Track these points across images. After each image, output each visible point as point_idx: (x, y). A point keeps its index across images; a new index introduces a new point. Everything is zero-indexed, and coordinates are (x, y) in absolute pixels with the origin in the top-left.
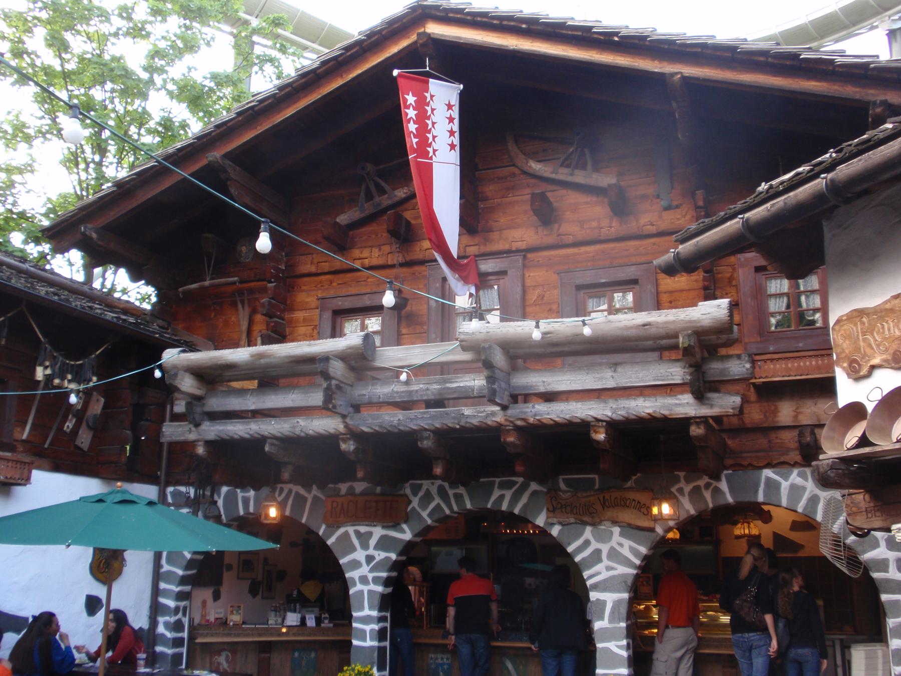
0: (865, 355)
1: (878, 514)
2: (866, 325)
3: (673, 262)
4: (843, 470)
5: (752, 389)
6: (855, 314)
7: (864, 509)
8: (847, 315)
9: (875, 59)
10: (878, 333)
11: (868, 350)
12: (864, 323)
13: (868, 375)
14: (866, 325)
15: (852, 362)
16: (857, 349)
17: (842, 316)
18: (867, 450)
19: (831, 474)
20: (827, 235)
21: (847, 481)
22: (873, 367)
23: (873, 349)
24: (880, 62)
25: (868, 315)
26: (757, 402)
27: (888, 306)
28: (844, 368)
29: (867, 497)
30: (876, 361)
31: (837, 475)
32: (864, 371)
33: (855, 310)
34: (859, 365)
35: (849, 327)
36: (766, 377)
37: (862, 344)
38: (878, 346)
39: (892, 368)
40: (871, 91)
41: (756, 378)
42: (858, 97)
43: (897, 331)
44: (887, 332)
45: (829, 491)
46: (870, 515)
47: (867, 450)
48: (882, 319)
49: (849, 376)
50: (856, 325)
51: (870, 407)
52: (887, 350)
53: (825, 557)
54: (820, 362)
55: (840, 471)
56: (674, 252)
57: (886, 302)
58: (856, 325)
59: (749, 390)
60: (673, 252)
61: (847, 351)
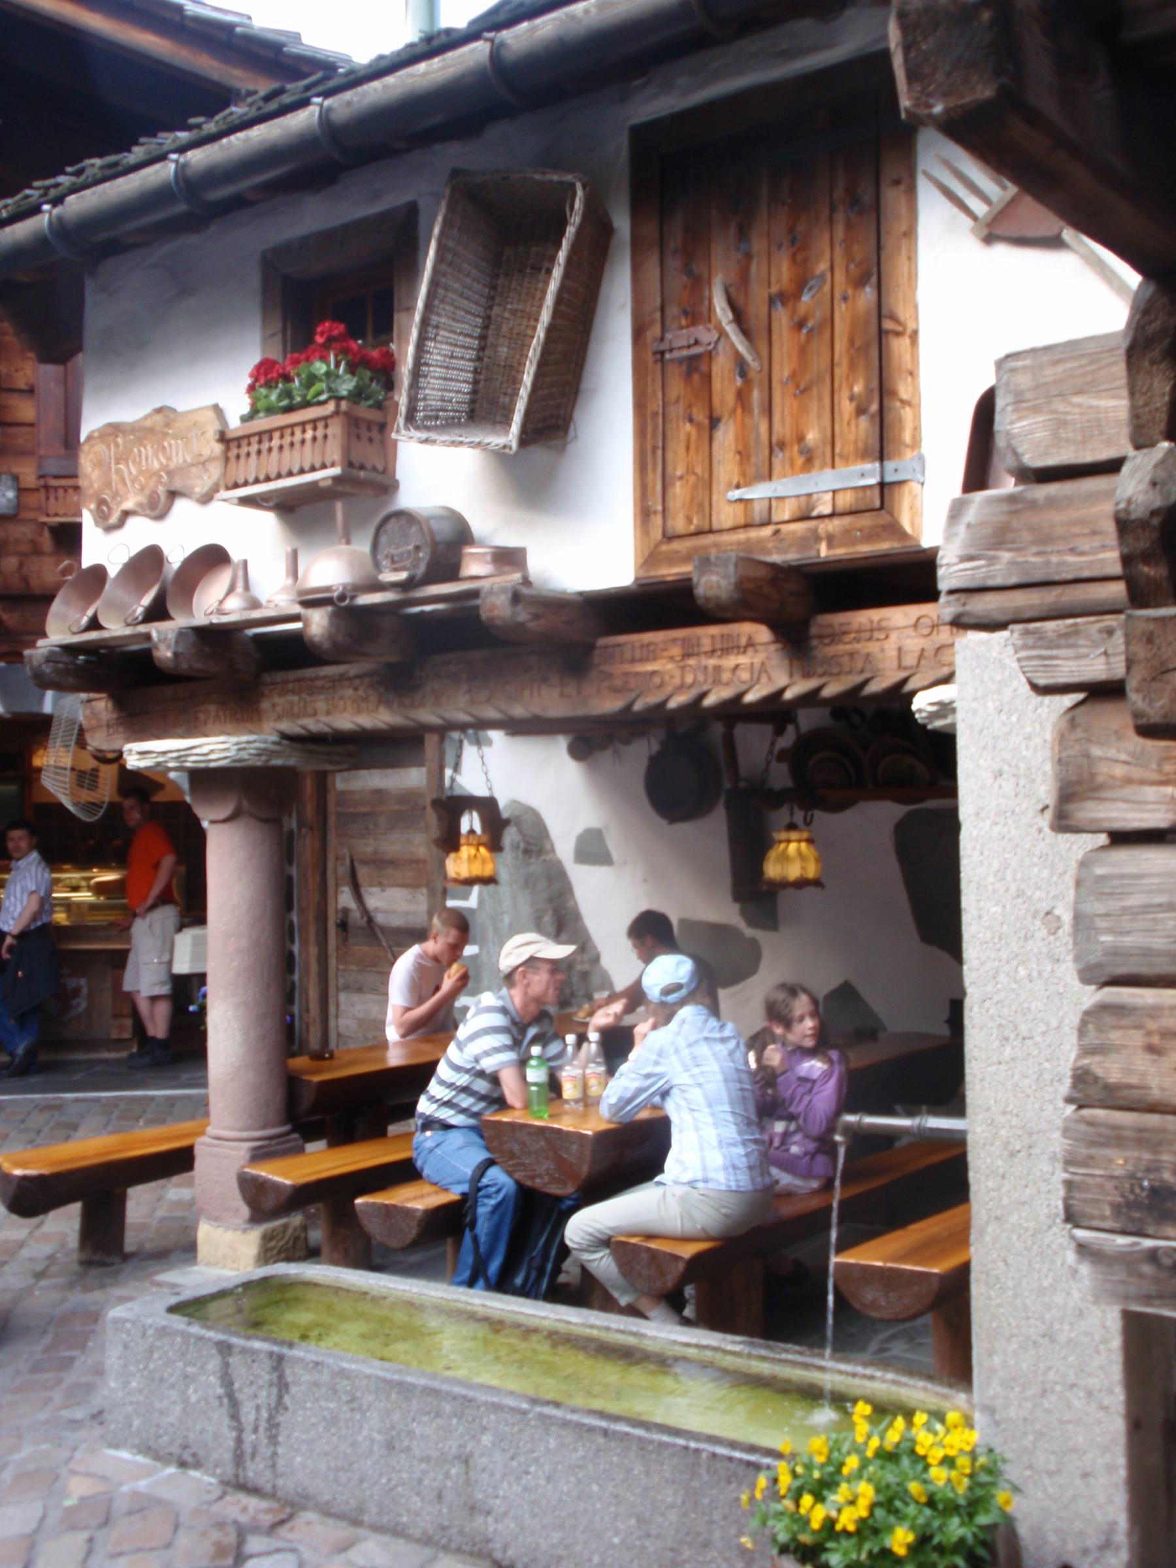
0: (116, 495)
1: (121, 729)
2: (121, 447)
3: (47, 231)
4: (65, 663)
5: (47, 533)
6: (110, 430)
7: (104, 722)
8: (99, 430)
9: (247, 21)
10: (134, 462)
11: (120, 487)
12: (117, 445)
13: (120, 524)
14: (121, 447)
15: (102, 502)
16: (108, 484)
17: (93, 431)
18: (93, 635)
19: (47, 669)
20: (89, 301)
21: (71, 680)
22: (126, 514)
23: (125, 484)
24: (250, 27)
25: (124, 432)
26: (52, 554)
27: (148, 423)
28: (91, 511)
29: (110, 705)
30: (129, 505)
31: (56, 671)
32: (114, 519)
33: (110, 425)
34: (109, 508)
35: (100, 448)
36: (65, 515)
37: (114, 477)
38: (133, 482)
39: (147, 516)
40: (237, 72)
41: (48, 515)
42: (215, 76)
43: (155, 462)
44: (144, 463)
45: (242, 734)
46: (111, 731)
47: (93, 635)
48: (140, 441)
49: (97, 524)
50: (108, 447)
51: (113, 571)
52: (142, 489)
53: (60, 806)
54: (1025, 447)
55: (60, 666)
56: (321, 105)
57: (146, 417)
58: (108, 447)
59: (41, 534)
60: (317, 104)
61: (96, 486)
